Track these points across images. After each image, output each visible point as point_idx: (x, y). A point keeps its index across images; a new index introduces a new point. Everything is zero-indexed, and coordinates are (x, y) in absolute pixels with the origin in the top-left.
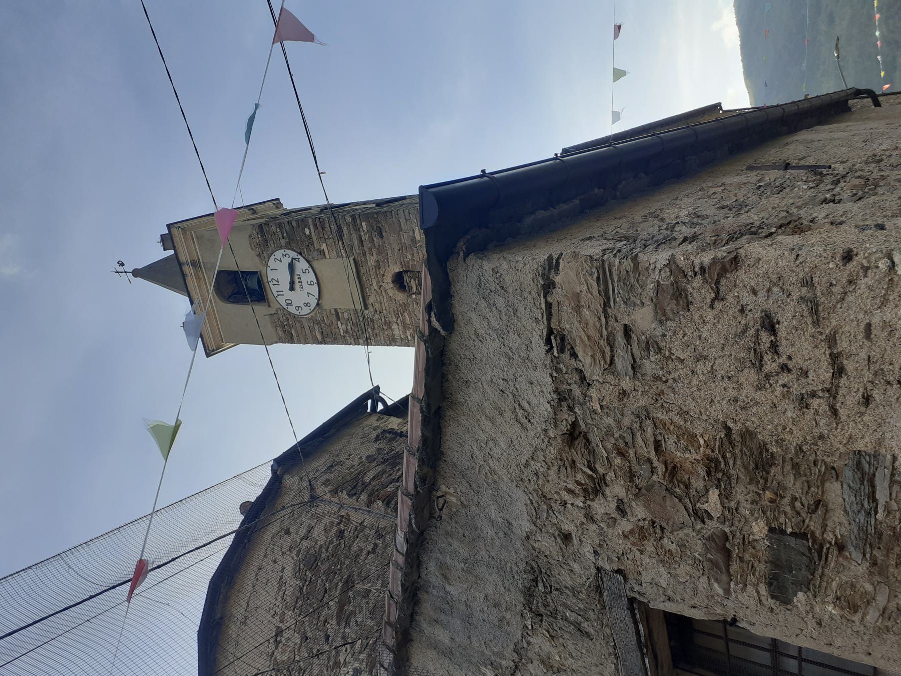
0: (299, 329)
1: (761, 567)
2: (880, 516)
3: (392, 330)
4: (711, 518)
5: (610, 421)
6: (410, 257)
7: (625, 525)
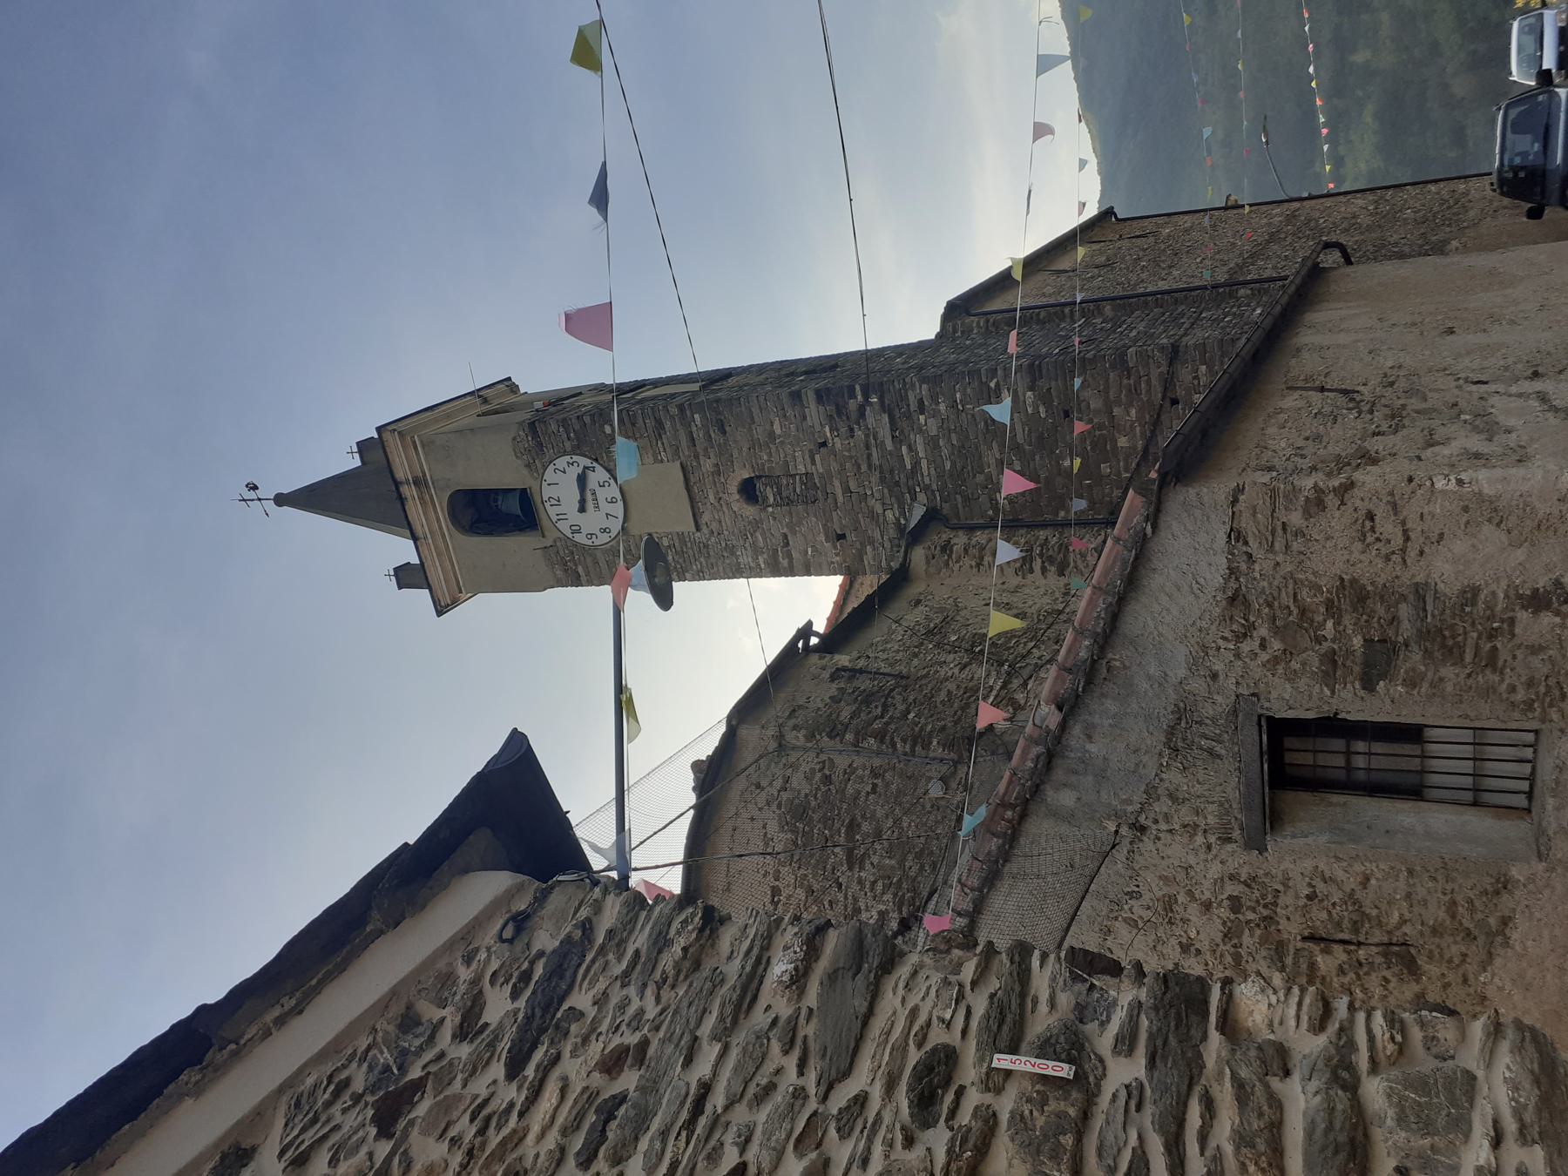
0: (590, 565)
1: (1357, 669)
2: (1429, 620)
4: (1326, 640)
5: (1265, 584)
6: (765, 457)
7: (1264, 657)
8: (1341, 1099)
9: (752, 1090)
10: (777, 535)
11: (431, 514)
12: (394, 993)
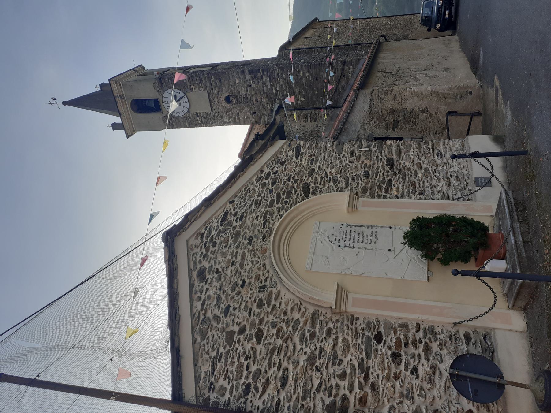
1: (392, 126)
3: (224, 119)
5: (376, 109)
6: (233, 90)
7: (375, 125)
8: (398, 148)
9: (330, 156)
10: (236, 113)
11: (125, 107)
12: (275, 153)
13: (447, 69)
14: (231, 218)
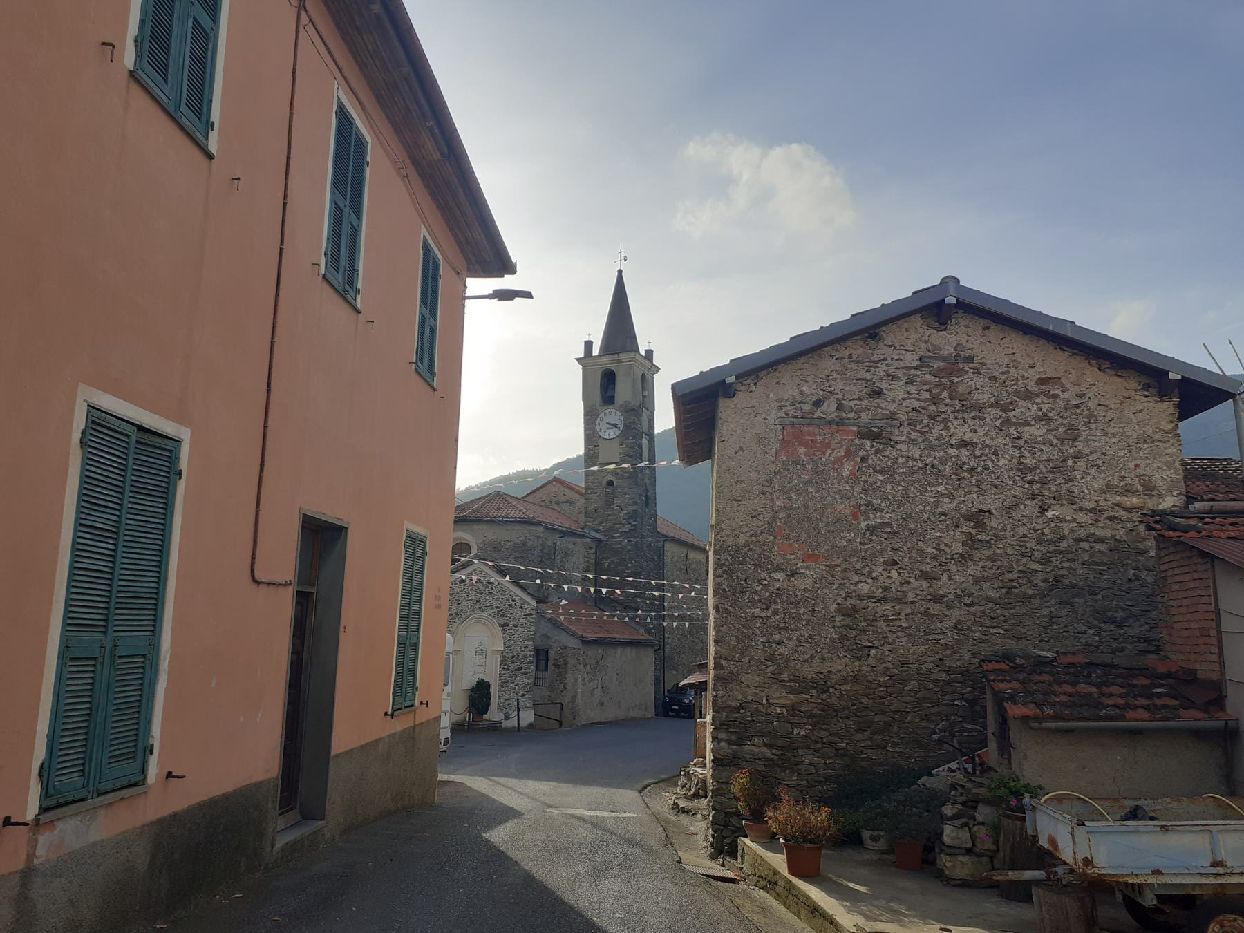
13: (602, 704)
14: (490, 586)
